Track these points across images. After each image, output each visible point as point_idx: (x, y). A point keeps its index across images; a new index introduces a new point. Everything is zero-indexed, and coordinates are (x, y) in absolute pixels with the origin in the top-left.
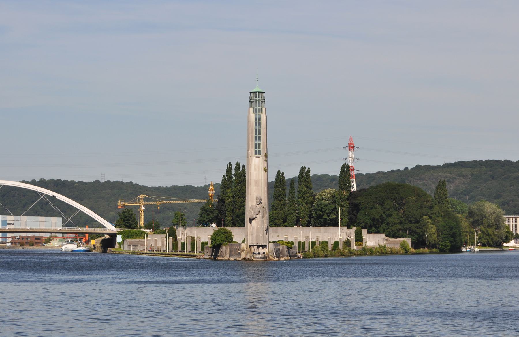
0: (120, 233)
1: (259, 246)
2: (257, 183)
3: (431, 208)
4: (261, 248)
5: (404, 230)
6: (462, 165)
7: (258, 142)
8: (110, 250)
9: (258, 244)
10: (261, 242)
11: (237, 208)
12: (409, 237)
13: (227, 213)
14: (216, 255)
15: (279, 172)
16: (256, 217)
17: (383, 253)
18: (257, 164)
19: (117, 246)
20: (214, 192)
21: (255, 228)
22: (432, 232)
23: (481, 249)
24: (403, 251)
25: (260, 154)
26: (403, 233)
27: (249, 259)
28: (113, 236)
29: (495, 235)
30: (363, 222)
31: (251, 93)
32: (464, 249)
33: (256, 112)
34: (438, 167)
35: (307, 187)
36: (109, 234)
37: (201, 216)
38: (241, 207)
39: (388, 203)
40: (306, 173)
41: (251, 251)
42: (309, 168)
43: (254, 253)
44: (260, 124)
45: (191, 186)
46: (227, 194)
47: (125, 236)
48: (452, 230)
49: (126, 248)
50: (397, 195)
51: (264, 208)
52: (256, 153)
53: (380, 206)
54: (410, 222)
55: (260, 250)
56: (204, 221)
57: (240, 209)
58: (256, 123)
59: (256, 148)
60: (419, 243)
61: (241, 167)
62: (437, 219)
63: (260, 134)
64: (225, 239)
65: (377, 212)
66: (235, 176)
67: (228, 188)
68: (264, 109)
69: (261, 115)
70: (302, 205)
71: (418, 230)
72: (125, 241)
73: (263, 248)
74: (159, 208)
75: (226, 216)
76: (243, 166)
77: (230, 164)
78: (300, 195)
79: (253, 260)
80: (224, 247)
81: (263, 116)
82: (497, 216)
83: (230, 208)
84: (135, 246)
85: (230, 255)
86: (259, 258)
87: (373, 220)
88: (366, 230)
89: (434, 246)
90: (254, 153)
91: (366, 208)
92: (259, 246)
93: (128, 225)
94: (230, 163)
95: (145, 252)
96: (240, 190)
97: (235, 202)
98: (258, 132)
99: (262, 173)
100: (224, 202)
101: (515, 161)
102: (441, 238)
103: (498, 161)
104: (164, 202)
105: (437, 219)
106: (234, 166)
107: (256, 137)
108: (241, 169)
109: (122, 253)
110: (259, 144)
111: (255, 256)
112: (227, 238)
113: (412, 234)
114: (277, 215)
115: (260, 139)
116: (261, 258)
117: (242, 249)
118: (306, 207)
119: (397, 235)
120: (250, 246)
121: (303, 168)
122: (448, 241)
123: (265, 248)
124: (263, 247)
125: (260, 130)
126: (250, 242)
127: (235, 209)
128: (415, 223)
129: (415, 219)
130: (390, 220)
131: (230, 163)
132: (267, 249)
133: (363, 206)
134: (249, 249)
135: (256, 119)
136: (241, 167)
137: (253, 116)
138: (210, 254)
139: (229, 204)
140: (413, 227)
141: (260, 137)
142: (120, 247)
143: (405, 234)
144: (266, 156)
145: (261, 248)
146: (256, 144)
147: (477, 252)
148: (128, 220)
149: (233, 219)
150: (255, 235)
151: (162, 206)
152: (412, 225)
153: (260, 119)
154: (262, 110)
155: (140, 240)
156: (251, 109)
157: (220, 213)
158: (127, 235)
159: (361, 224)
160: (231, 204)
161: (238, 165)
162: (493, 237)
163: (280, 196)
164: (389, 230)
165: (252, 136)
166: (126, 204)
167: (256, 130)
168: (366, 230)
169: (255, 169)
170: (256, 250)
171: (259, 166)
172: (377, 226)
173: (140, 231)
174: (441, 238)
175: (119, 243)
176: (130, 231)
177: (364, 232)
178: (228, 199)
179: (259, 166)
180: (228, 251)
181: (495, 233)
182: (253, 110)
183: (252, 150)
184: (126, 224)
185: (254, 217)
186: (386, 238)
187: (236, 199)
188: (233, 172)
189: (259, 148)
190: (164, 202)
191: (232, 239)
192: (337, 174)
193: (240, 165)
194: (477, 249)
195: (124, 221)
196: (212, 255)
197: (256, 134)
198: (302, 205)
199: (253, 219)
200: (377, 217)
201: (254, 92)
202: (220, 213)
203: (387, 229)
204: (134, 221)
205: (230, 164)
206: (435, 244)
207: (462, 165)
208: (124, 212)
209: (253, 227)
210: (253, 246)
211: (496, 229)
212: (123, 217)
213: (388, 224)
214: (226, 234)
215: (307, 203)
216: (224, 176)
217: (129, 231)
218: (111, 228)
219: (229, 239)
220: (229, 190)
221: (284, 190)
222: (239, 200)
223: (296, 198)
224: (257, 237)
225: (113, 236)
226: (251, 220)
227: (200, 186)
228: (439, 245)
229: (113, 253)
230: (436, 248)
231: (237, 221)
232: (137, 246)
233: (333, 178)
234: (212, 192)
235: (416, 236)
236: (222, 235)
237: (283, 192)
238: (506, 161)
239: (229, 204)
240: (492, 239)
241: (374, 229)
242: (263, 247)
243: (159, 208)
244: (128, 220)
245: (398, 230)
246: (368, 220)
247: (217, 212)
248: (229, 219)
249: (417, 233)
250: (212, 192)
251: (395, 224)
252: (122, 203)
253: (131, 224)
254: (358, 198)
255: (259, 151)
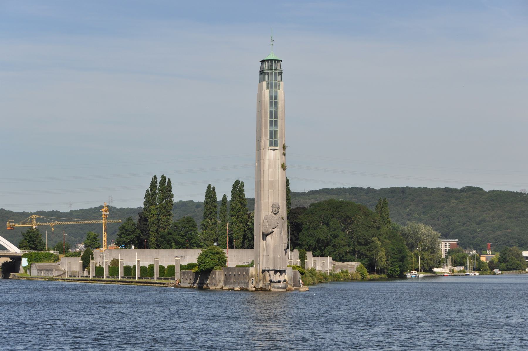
0: (25, 256)
1: (276, 271)
2: (272, 184)
3: (378, 228)
4: (278, 274)
5: (353, 252)
6: (326, 192)
7: (274, 129)
8: (14, 276)
9: (276, 269)
10: (279, 266)
11: (163, 228)
12: (358, 261)
13: (150, 232)
14: (202, 283)
15: (209, 187)
16: (272, 232)
17: (345, 279)
18: (272, 159)
19: (22, 270)
20: (108, 213)
21: (272, 246)
22: (382, 257)
23: (425, 275)
24: (360, 277)
25: (276, 145)
26: (351, 257)
27: (263, 290)
28: (17, 260)
29: (431, 260)
30: (307, 244)
31: (263, 61)
32: (409, 275)
33: (271, 87)
34: (303, 194)
35: (241, 204)
36: (12, 257)
37: (120, 236)
38: (166, 226)
39: (335, 223)
40: (240, 188)
41: (264, 277)
42: (242, 182)
43: (271, 281)
44: (276, 103)
45: (57, 211)
46: (150, 211)
47: (32, 260)
48: (400, 253)
49: (34, 272)
50: (342, 214)
51: (283, 218)
52: (271, 144)
53: (325, 226)
54: (360, 244)
55: (278, 277)
56: (124, 243)
57: (165, 229)
58: (271, 103)
59: (271, 137)
60: (371, 267)
61: (167, 180)
62: (385, 240)
63: (276, 117)
64: (216, 261)
65: (323, 232)
66: (159, 191)
67: (152, 205)
68: (282, 84)
69: (278, 91)
70: (236, 224)
71: (368, 254)
72: (33, 265)
73: (281, 274)
74: (53, 229)
75: (149, 237)
76: (169, 180)
77: (155, 178)
78: (233, 213)
79: (270, 291)
80: (217, 272)
81: (281, 93)
82: (433, 238)
83: (153, 228)
84: (47, 270)
85: (225, 284)
86: (279, 288)
87: (318, 241)
88: (311, 253)
89: (382, 271)
90: (268, 143)
91: (309, 228)
92: (276, 271)
93: (33, 246)
94: (155, 176)
95: (67, 277)
96: (165, 207)
97: (159, 221)
98: (274, 115)
99: (280, 171)
100: (147, 221)
101: (378, 189)
102: (389, 262)
103: (361, 189)
104: (58, 223)
105: (385, 240)
106: (159, 180)
107: (271, 122)
108: (166, 183)
109: (31, 279)
110: (276, 132)
111: (273, 285)
112: (219, 260)
113: (360, 257)
114: (207, 235)
115: (276, 124)
116: (282, 288)
117: (250, 275)
118: (241, 227)
119: (344, 258)
120: (263, 271)
121: (237, 182)
122: (397, 266)
123: (284, 274)
124: (281, 272)
125: (276, 112)
126: (263, 265)
127: (160, 229)
128: (365, 245)
129: (366, 240)
130: (337, 241)
131: (155, 176)
132: (286, 276)
133: (305, 226)
134: (261, 275)
135: (271, 97)
136: (167, 180)
137: (266, 93)
138: (192, 281)
139: (153, 223)
140: (364, 249)
141: (276, 122)
142: (26, 272)
143: (353, 257)
144: (284, 148)
145: (278, 274)
146: (271, 132)
147: (422, 278)
148: (33, 241)
149: (157, 240)
150: (271, 256)
151: (56, 227)
152: (362, 247)
153: (276, 98)
154: (279, 85)
155: (51, 264)
156: (265, 84)
157: (142, 232)
158: (34, 258)
159: (304, 246)
160: (155, 222)
161: (163, 177)
162: (429, 261)
163: (211, 213)
164: (335, 253)
165: (266, 121)
166: (16, 226)
167: (271, 112)
168: (311, 253)
169: (269, 165)
170: (272, 277)
171: (275, 162)
172: (323, 248)
173: (49, 253)
174: (389, 262)
175: (24, 268)
176: (38, 253)
177: (309, 254)
178: (152, 217)
179: (275, 162)
180: (223, 278)
181: (431, 257)
182: (268, 84)
183: (266, 140)
184: (31, 245)
185: (270, 231)
186: (333, 261)
187: (161, 217)
188: (158, 187)
189: (275, 138)
190: (58, 223)
191: (225, 261)
192: (202, 199)
193: (165, 179)
194: (421, 275)
195: (28, 242)
196: (194, 283)
197: (271, 117)
198: (236, 224)
199: (267, 235)
200: (323, 237)
201: (268, 61)
202: (142, 232)
203: (333, 252)
204: (40, 243)
205: (155, 178)
206: (383, 269)
207: (326, 192)
208: (29, 232)
209: (268, 246)
210: (268, 271)
211: (431, 253)
212: (28, 238)
213: (334, 246)
214: (218, 256)
215: (241, 222)
216: (147, 191)
217: (36, 253)
218: (13, 249)
219: (222, 261)
220: (153, 207)
221: (215, 207)
222: (165, 218)
223: (228, 217)
224: (274, 258)
225: (17, 260)
226: (265, 236)
227: (65, 211)
228: (388, 270)
229: (19, 279)
230: (384, 273)
231: (162, 242)
232: (52, 270)
233: (198, 205)
234: (106, 213)
235: (366, 259)
236: (212, 257)
237: (215, 209)
238: (369, 188)
239: (153, 223)
240: (428, 264)
241: (318, 251)
242: (281, 272)
243: (53, 229)
244: (33, 241)
245: (346, 253)
246: (312, 242)
247: (139, 232)
248: (153, 239)
249: (366, 256)
250: (106, 213)
251: (344, 246)
252: (11, 224)
253: (36, 246)
254: (300, 217)
255: (276, 141)
